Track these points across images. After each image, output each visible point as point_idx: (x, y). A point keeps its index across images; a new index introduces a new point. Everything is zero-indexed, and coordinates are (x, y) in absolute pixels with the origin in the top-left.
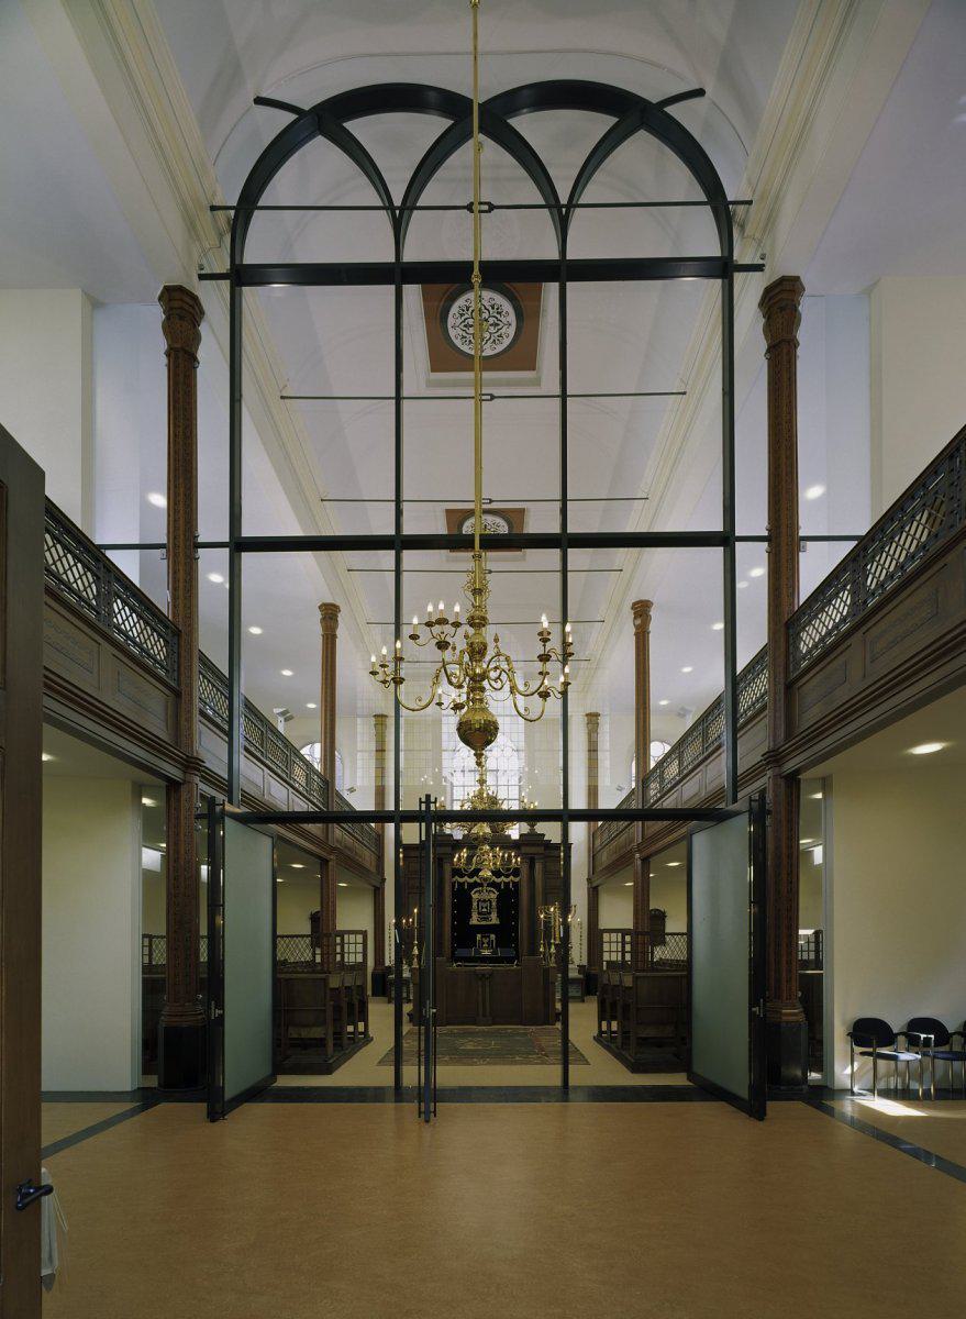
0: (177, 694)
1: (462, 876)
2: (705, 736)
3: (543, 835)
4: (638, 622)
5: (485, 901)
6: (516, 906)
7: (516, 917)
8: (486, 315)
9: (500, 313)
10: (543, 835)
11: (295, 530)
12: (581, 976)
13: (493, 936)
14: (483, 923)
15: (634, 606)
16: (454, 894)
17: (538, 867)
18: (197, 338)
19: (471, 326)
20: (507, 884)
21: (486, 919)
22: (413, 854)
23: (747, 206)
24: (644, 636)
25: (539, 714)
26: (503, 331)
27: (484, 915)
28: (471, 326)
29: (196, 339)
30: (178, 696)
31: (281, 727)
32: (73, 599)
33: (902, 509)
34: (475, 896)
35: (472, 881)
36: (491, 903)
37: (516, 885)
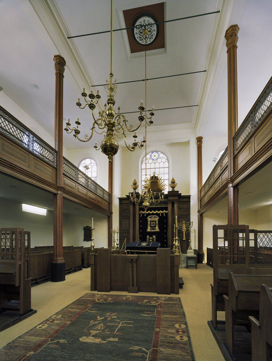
0: (56, 169)
1: (143, 210)
3: (178, 192)
4: (198, 143)
5: (153, 221)
6: (167, 223)
7: (167, 229)
10: (178, 192)
12: (195, 256)
13: (154, 236)
14: (153, 231)
16: (140, 219)
17: (176, 206)
18: (64, 69)
19: (142, 33)
20: (162, 214)
21: (154, 229)
22: (124, 202)
25: (84, 107)
26: (152, 33)
27: (153, 228)
28: (142, 33)
29: (63, 70)
30: (56, 169)
32: (47, 160)
33: (259, 101)
34: (149, 219)
35: (147, 213)
36: (156, 222)
37: (166, 214)
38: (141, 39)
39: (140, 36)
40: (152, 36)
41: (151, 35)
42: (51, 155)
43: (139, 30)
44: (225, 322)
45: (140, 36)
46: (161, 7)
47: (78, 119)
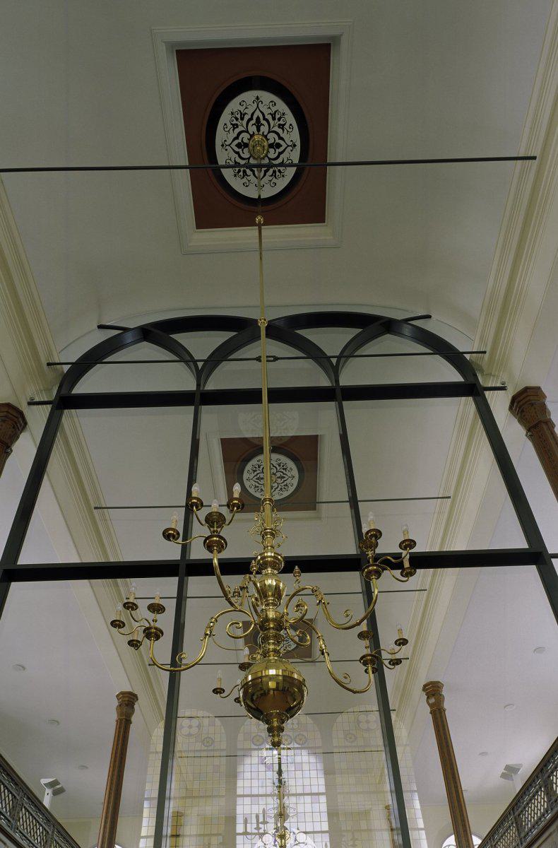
2: (518, 822)
4: (432, 701)
8: (275, 471)
9: (285, 469)
11: (70, 557)
15: (425, 688)
23: (483, 355)
24: (440, 713)
25: (357, 689)
31: (47, 801)
38: (279, 119)
39: (280, 131)
40: (235, 126)
41: (237, 131)
42: (11, 799)
43: (279, 161)
44: (178, 565)
45: (280, 131)
46: (207, 217)
47: (400, 631)
